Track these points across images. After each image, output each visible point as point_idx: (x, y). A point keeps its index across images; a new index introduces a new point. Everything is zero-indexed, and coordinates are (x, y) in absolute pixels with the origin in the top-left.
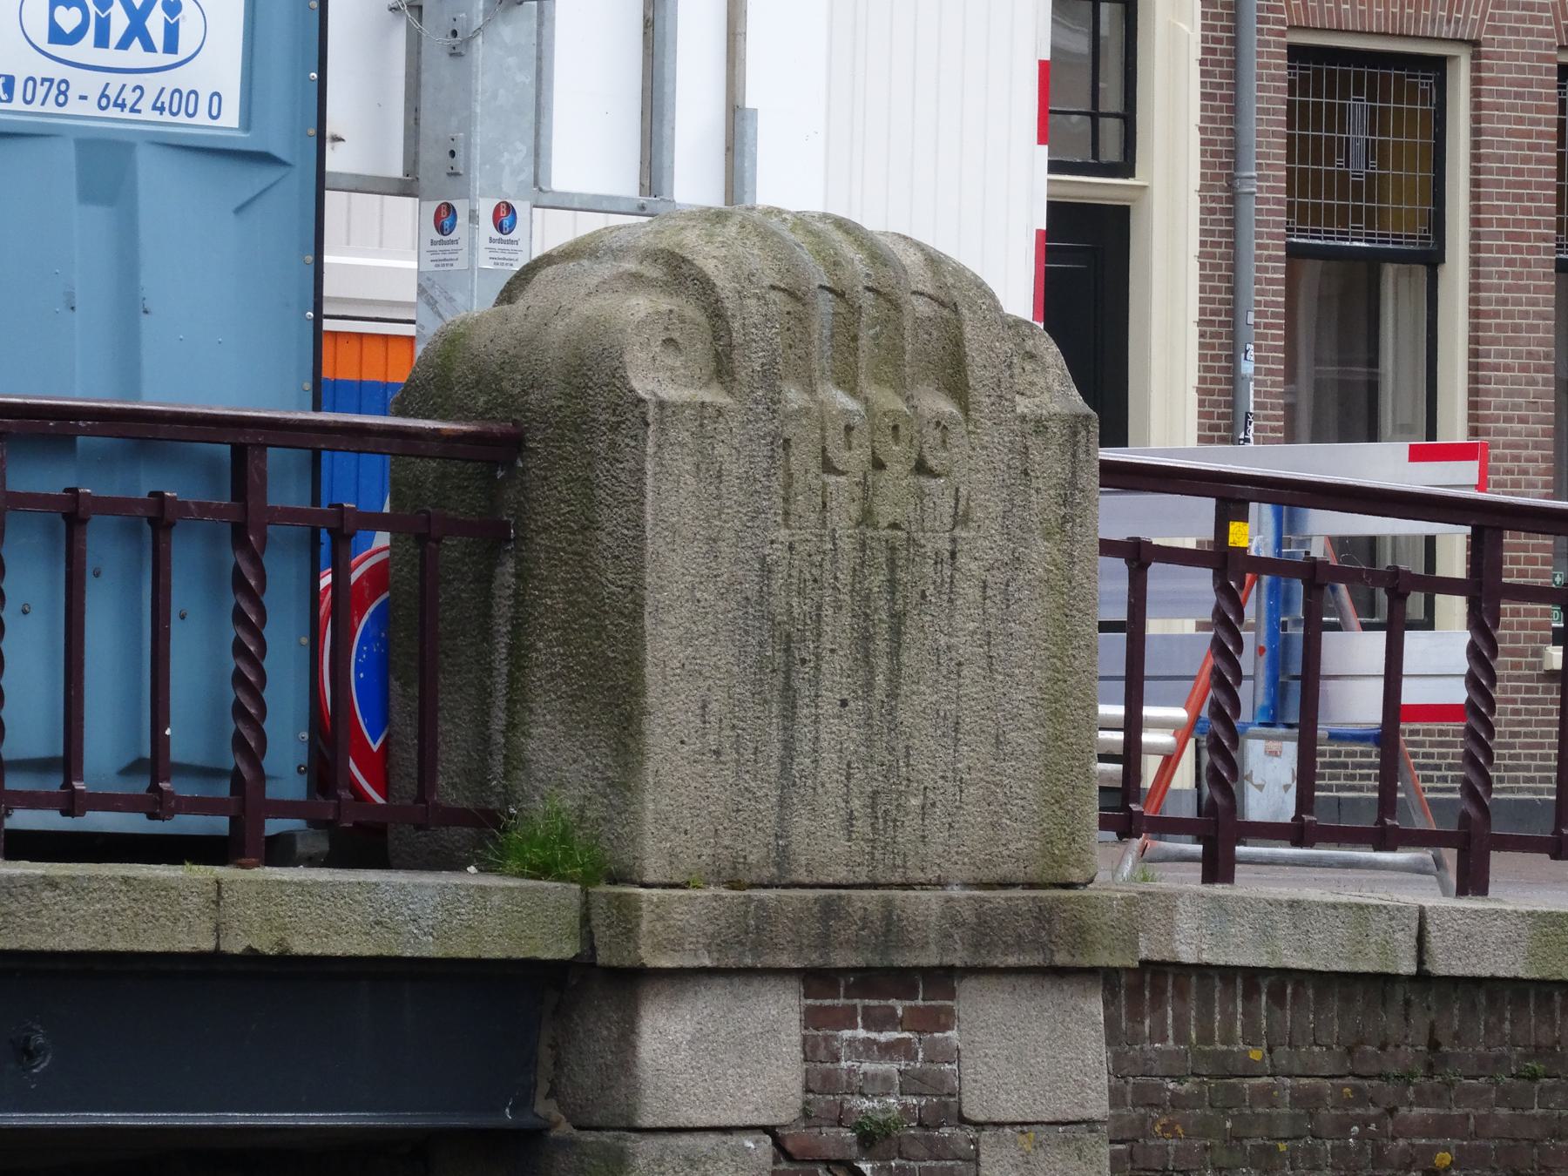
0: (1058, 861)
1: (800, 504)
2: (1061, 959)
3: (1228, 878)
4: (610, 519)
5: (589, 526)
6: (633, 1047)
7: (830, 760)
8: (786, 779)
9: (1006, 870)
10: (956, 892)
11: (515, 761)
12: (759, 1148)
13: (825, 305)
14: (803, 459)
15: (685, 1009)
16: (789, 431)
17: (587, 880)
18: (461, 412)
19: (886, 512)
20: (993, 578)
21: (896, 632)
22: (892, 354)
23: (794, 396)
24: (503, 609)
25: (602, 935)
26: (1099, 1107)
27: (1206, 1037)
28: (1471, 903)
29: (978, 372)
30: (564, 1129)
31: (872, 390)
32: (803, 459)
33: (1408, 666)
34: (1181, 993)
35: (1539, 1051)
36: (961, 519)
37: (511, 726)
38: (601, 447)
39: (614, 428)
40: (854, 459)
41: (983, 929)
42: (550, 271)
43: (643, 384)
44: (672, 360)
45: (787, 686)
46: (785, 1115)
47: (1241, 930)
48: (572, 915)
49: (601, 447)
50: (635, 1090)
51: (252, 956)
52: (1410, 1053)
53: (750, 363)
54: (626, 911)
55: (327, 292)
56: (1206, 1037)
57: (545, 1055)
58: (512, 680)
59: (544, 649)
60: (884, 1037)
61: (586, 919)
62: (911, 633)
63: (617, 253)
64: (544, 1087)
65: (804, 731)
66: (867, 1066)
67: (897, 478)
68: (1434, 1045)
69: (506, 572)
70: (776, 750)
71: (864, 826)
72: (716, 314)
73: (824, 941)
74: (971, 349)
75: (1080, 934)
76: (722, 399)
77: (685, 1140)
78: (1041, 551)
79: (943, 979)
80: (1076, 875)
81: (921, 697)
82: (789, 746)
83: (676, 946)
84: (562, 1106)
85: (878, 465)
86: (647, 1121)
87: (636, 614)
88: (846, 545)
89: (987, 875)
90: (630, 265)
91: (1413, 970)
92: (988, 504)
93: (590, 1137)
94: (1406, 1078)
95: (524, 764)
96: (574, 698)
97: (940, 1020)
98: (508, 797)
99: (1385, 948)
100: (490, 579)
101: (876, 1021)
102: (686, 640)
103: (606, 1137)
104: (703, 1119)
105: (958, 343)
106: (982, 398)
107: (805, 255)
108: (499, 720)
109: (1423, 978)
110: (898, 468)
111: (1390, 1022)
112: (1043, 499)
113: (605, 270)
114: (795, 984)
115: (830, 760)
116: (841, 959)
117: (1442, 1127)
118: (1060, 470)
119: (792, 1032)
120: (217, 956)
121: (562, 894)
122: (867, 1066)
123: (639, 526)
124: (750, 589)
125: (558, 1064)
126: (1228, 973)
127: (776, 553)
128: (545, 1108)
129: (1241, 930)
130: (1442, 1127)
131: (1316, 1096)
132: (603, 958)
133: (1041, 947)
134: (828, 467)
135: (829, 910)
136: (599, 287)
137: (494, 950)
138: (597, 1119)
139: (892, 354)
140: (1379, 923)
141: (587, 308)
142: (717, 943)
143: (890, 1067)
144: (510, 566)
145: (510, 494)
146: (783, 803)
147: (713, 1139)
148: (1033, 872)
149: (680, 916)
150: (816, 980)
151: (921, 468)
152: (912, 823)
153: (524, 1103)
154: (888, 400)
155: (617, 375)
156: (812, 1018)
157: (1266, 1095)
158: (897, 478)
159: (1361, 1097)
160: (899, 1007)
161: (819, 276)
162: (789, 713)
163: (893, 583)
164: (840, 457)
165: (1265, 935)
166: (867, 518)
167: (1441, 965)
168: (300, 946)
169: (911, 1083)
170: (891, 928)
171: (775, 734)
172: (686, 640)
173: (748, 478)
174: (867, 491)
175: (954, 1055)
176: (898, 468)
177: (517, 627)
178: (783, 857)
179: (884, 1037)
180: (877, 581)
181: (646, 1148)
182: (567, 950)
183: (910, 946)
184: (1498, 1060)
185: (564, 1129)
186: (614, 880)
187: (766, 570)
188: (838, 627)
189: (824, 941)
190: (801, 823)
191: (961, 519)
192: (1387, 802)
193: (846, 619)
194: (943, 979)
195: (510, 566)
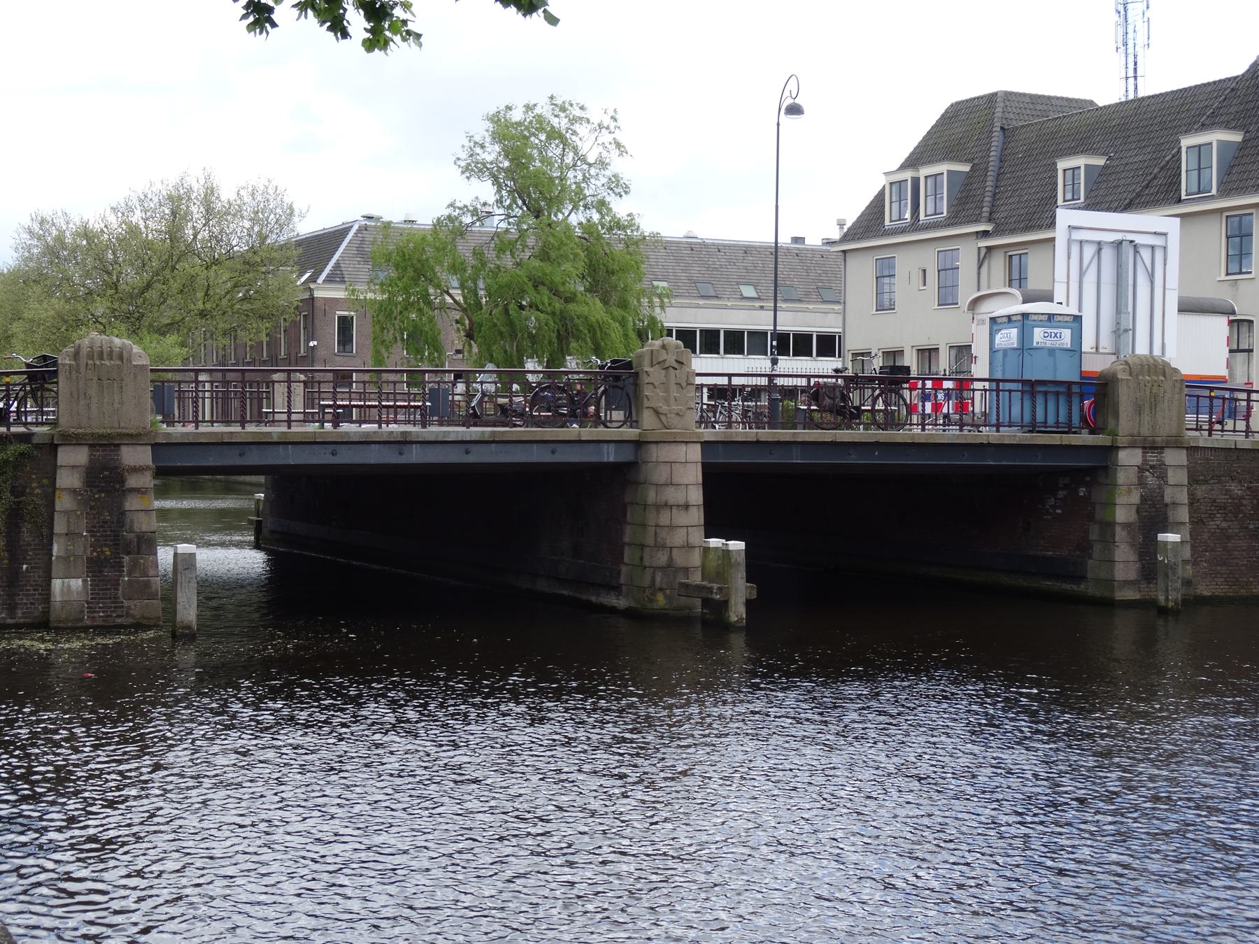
14: (1142, 385)
40: (1150, 385)
150: (1144, 448)
188: (1147, 405)
194: (1162, 448)
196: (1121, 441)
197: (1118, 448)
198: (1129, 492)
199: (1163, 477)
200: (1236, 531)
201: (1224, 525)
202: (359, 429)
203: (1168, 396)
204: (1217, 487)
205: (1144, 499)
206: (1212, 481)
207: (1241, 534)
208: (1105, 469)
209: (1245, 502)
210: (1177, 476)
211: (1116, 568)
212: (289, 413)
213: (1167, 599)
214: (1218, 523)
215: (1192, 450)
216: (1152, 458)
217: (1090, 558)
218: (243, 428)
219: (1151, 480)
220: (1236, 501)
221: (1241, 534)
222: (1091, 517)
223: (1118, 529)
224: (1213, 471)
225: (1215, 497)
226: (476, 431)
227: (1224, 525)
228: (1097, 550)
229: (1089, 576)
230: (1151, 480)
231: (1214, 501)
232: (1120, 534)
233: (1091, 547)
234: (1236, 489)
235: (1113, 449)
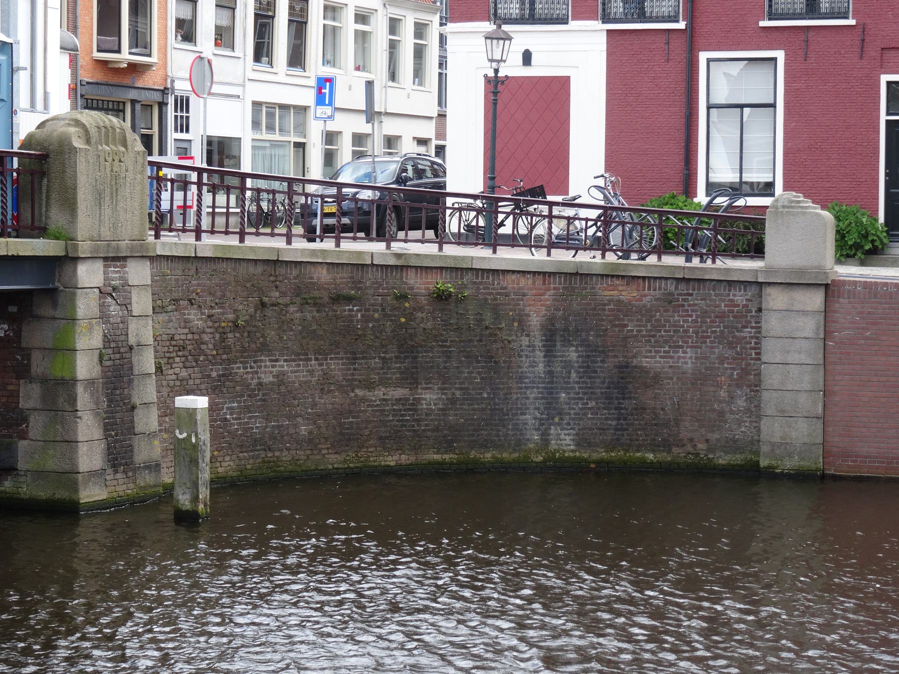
0: (142, 236)
1: (102, 168)
2: (144, 254)
3: (200, 240)
4: (69, 171)
5: (64, 172)
6: (76, 272)
7: (107, 217)
8: (100, 221)
9: (134, 238)
10: (127, 242)
11: (47, 217)
12: (97, 291)
13: (103, 129)
14: (102, 159)
15: (85, 265)
16: (100, 154)
17: (65, 240)
18: (35, 150)
19: (115, 169)
20: (132, 182)
21: (117, 192)
22: (114, 139)
23: (100, 147)
24: (44, 188)
25: (70, 251)
26: (149, 283)
27: (161, 269)
28: (289, 247)
29: (129, 143)
30: (62, 288)
31: (111, 146)
32: (102, 159)
33: (169, 202)
34: (157, 261)
35: (214, 270)
36: (127, 171)
37: (47, 211)
38: (67, 157)
39: (70, 153)
40: (110, 159)
41: (132, 249)
42: (50, 122)
43: (76, 144)
44: (79, 140)
45: (100, 203)
46: (101, 285)
47: (167, 248)
48: (64, 247)
49: (67, 157)
50: (77, 281)
51: (13, 256)
52: (193, 272)
53: (93, 141)
54: (76, 248)
55: (189, 82)
56: (161, 269)
57: (57, 274)
58: (47, 202)
59: (54, 195)
60: (116, 269)
61: (66, 248)
62: (119, 193)
63: (63, 119)
64: (57, 280)
65: (103, 212)
66: (114, 275)
67: (116, 162)
68: (197, 270)
69: (45, 181)
70: (98, 215)
71: (112, 229)
72: (86, 131)
73: (108, 252)
74: (128, 138)
75: (147, 250)
76: (89, 148)
77: (85, 290)
78: (139, 176)
79: (125, 258)
80: (145, 238)
81: (121, 204)
82: (100, 215)
83: (84, 253)
84: (61, 284)
85: (114, 160)
86: (79, 287)
87: (75, 189)
88: (109, 175)
89: (132, 238)
90: (67, 122)
91: (370, 263)
92: (131, 168)
93: (67, 290)
94: (193, 276)
95: (50, 218)
96: (61, 205)
97: (124, 266)
98: (46, 224)
99: (190, 252)
100: (41, 182)
101: (115, 267)
102: (84, 194)
103: (71, 290)
104: (88, 286)
105: (125, 137)
106: (129, 147)
107: (99, 120)
108: (44, 209)
109: (373, 265)
110: (117, 161)
111: (190, 265)
112: (139, 167)
113: (63, 122)
114: (102, 260)
115: (107, 217)
116: (111, 255)
117: (199, 285)
118: (142, 161)
119: (102, 269)
120: (7, 255)
121: (62, 243)
122: (114, 275)
123: (76, 172)
124: (94, 184)
125: (60, 276)
126: (164, 256)
127: (98, 177)
128: (57, 284)
129: (167, 248)
130: (199, 285)
131: (178, 279)
132: (70, 255)
133: (141, 252)
134: (106, 161)
135: (108, 245)
136: (63, 126)
137: (51, 254)
138: (69, 286)
139: (114, 139)
140: (189, 247)
141: (61, 129)
142: (91, 252)
143: (117, 275)
144: (46, 180)
145: (45, 166)
146: (99, 225)
147: (90, 290)
148: (138, 238)
149: (85, 247)
150: (106, 259)
151: (120, 161)
152: (119, 228)
153: (53, 284)
154: (114, 148)
155: (70, 144)
156: (105, 266)
157: (171, 279)
158: (116, 162)
159: (186, 280)
160: (118, 264)
161: (102, 124)
162: (100, 208)
163: (116, 183)
164: (108, 159)
165: (171, 249)
166: (112, 171)
167: (199, 255)
168: (21, 254)
169: (121, 278)
170: (118, 249)
171: (98, 212)
172: (84, 194)
173: (93, 163)
174: (112, 165)
175: (127, 273)
176: (117, 161)
177: (48, 192)
178: (100, 235)
179: (116, 269)
180: (113, 183)
181: (79, 291)
182: (63, 254)
183: (121, 252)
184: (207, 272)
185: (62, 288)
186: (71, 240)
187: (96, 181)
188: (108, 191)
189: (108, 252)
190: (102, 229)
191: (127, 171)
192: (550, 223)
193: (109, 190)
194: (125, 258)
195: (46, 180)
196: (84, 248)
197: (76, 260)
198: (90, 329)
199: (126, 305)
200: (198, 381)
201: (184, 373)
202: (530, 257)
203: (130, 175)
204: (175, 316)
205: (106, 340)
206: (170, 308)
207: (203, 386)
208: (51, 294)
209: (206, 338)
210: (142, 303)
211: (80, 452)
212: (228, 207)
213: (195, 499)
214: (177, 370)
215: (154, 259)
216: (114, 272)
217: (23, 436)
218: (495, 252)
219: (114, 309)
220: (196, 337)
221: (203, 386)
222: (23, 372)
223: (80, 390)
224: (170, 291)
225: (173, 331)
226: (562, 256)
227: (184, 373)
228: (36, 425)
229: (21, 465)
230: (114, 309)
231: (172, 339)
232: (83, 398)
233: (25, 420)
234: (195, 318)
235: (69, 260)
